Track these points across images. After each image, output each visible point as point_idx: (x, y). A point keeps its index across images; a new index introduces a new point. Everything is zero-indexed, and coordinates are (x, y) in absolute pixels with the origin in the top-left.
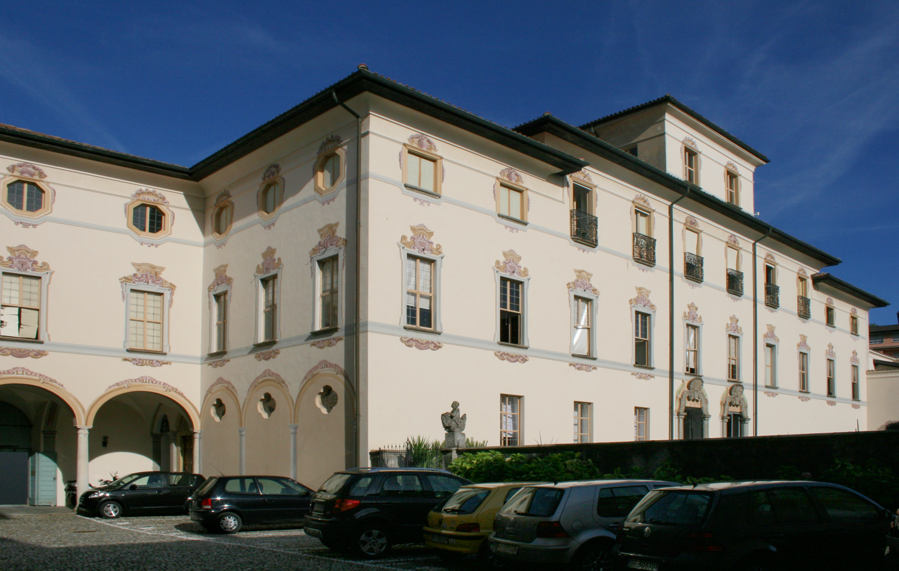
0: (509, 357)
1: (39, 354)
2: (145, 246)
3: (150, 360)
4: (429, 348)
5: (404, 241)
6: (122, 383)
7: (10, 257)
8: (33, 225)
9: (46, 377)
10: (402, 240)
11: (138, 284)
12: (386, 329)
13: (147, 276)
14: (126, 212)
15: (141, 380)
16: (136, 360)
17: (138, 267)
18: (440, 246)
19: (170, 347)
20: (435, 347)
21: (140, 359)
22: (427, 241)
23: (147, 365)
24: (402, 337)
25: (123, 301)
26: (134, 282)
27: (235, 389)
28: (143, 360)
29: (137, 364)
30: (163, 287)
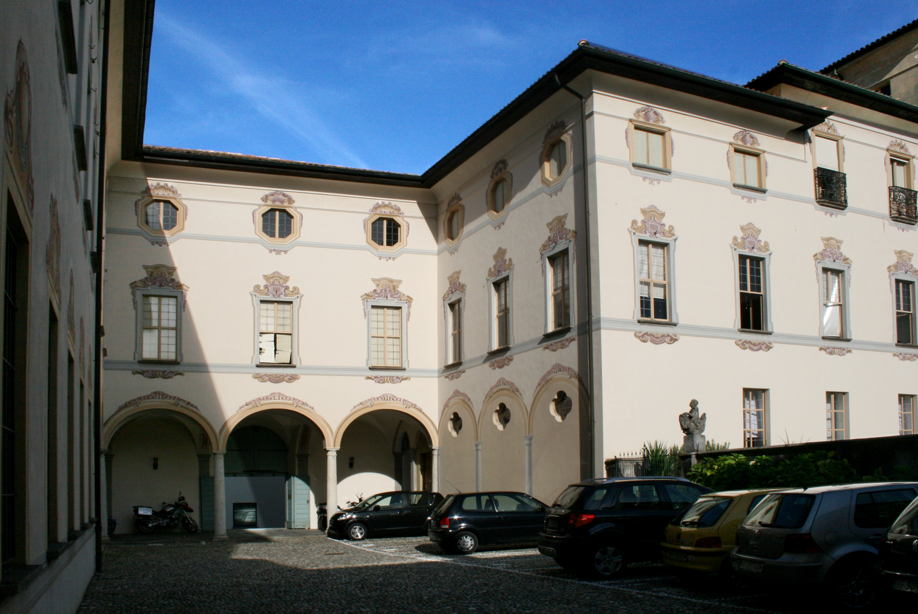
0: (751, 346)
1: (293, 378)
2: (384, 260)
3: (390, 377)
4: (665, 341)
5: (635, 226)
6: (366, 402)
7: (266, 285)
8: (285, 251)
9: (299, 401)
10: (632, 225)
11: (378, 299)
12: (620, 325)
13: (386, 291)
14: (365, 228)
15: (384, 398)
16: (378, 378)
17: (378, 283)
18: (672, 227)
19: (408, 361)
20: (671, 340)
21: (152, 371)
22: (659, 224)
23: (388, 382)
24: (636, 332)
25: (365, 318)
26: (374, 299)
27: (192, 405)
28: (384, 377)
29: (378, 382)
30: (401, 300)
